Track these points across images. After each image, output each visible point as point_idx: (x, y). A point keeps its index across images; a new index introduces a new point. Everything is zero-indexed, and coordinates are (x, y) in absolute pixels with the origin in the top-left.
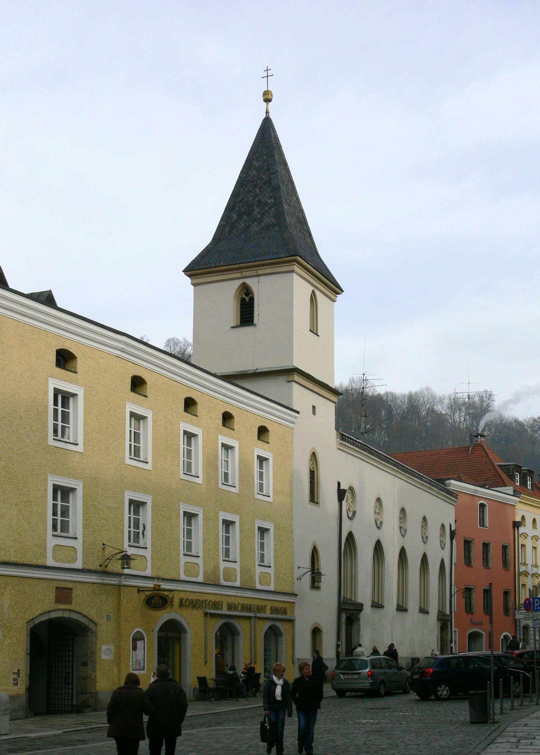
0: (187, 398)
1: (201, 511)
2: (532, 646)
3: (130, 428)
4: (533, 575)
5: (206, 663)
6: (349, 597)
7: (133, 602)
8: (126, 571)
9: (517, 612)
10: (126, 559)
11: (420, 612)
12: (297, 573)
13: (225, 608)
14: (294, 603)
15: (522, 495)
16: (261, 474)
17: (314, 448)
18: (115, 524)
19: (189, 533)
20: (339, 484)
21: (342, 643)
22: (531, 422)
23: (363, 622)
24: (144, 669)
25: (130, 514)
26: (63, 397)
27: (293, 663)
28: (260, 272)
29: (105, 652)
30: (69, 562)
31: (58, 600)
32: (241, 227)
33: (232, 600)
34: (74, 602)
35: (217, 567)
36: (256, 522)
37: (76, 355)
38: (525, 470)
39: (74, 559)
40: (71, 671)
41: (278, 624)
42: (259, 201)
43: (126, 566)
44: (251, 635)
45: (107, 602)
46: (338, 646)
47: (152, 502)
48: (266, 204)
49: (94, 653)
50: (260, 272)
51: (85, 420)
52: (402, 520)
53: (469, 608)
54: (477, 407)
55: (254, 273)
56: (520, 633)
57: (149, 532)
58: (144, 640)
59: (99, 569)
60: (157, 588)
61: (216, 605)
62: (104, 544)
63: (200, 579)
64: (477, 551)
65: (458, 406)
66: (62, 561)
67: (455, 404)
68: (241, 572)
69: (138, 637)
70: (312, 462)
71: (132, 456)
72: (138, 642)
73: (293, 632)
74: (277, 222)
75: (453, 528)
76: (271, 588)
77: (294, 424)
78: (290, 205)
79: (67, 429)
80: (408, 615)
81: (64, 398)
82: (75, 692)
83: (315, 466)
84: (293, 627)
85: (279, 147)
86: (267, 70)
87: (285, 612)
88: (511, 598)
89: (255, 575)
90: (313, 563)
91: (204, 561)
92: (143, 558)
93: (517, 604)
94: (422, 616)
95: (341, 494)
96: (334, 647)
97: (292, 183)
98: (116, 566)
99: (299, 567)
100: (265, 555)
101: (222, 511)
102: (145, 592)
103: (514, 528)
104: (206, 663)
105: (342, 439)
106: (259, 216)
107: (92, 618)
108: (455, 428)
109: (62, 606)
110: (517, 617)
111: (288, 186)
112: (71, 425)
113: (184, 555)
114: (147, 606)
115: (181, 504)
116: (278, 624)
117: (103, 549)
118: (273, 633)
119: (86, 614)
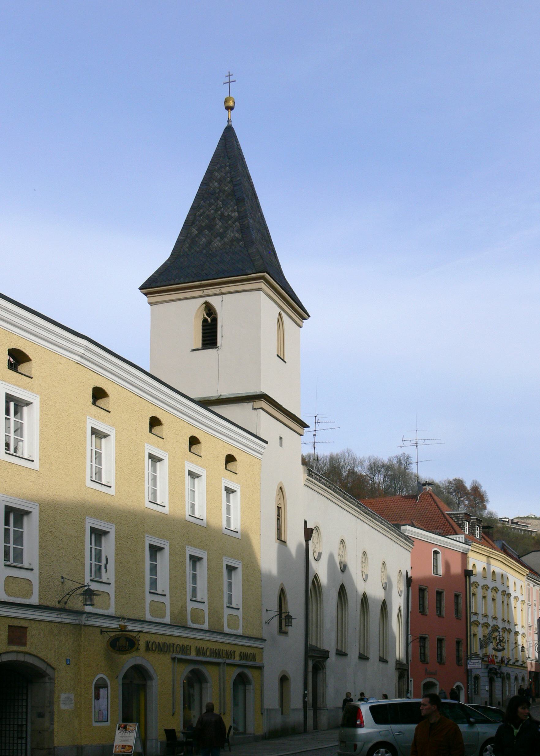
0: (153, 417)
1: (168, 544)
2: (271, 699)
3: (91, 446)
4: (483, 624)
5: (173, 714)
6: (314, 644)
7: (97, 645)
8: (88, 609)
9: (469, 661)
10: (89, 595)
11: (380, 661)
12: (266, 617)
13: (193, 653)
14: (262, 648)
15: (473, 543)
16: (228, 507)
17: (281, 482)
18: (76, 554)
19: (154, 569)
20: (306, 522)
21: (308, 692)
22: (447, 485)
23: (328, 671)
24: (107, 721)
25: (91, 544)
26: (16, 406)
27: (262, 714)
28: (224, 290)
29: (64, 701)
30: (24, 597)
31: (11, 641)
32: (201, 243)
33: (200, 645)
34: (28, 643)
35: (184, 608)
36: (224, 560)
37: (30, 357)
38: (474, 519)
39: (29, 594)
40: (24, 723)
41: (246, 671)
42: (222, 215)
43: (88, 603)
44: (220, 683)
45: (67, 644)
46: (305, 696)
47: (116, 531)
48: (230, 217)
49: (51, 703)
50: (224, 290)
51: (41, 434)
52: (364, 565)
53: (423, 659)
54: (395, 470)
55: (217, 291)
56: (471, 683)
57: (111, 566)
58: (107, 687)
59: (58, 606)
60: (123, 629)
61: (185, 649)
62: (62, 578)
63: (167, 620)
64: (430, 599)
65: (377, 468)
66: (16, 596)
67: (375, 467)
68: (209, 613)
69: (100, 685)
70: (279, 497)
71: (94, 479)
72: (101, 690)
73: (262, 680)
74: (243, 237)
75: (409, 575)
76: (240, 632)
77: (262, 454)
78: (254, 220)
79: (20, 443)
80: (369, 663)
81: (15, 405)
82: (29, 747)
83: (282, 501)
84: (262, 674)
85: (243, 158)
86: (229, 76)
87: (253, 658)
88: (462, 648)
89: (223, 617)
90: (280, 606)
91: (171, 601)
92: (106, 594)
93: (469, 654)
94: (381, 665)
95: (308, 533)
96: (301, 698)
97: (256, 198)
98: (77, 603)
99: (267, 610)
100: (233, 596)
101: (189, 545)
102: (108, 633)
103: (466, 577)
104: (173, 714)
105: (309, 475)
106: (221, 230)
107: (49, 662)
108: (375, 488)
109: (15, 648)
110: (469, 667)
111: (252, 200)
112: (25, 438)
113: (150, 593)
114: (111, 649)
115: (146, 535)
116: (246, 671)
117: (62, 583)
118: (242, 681)
119: (42, 657)
